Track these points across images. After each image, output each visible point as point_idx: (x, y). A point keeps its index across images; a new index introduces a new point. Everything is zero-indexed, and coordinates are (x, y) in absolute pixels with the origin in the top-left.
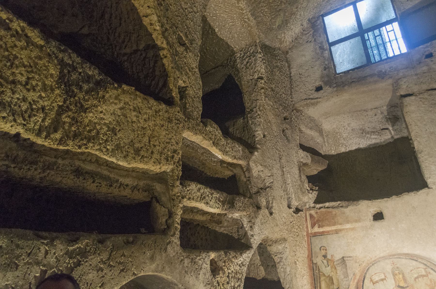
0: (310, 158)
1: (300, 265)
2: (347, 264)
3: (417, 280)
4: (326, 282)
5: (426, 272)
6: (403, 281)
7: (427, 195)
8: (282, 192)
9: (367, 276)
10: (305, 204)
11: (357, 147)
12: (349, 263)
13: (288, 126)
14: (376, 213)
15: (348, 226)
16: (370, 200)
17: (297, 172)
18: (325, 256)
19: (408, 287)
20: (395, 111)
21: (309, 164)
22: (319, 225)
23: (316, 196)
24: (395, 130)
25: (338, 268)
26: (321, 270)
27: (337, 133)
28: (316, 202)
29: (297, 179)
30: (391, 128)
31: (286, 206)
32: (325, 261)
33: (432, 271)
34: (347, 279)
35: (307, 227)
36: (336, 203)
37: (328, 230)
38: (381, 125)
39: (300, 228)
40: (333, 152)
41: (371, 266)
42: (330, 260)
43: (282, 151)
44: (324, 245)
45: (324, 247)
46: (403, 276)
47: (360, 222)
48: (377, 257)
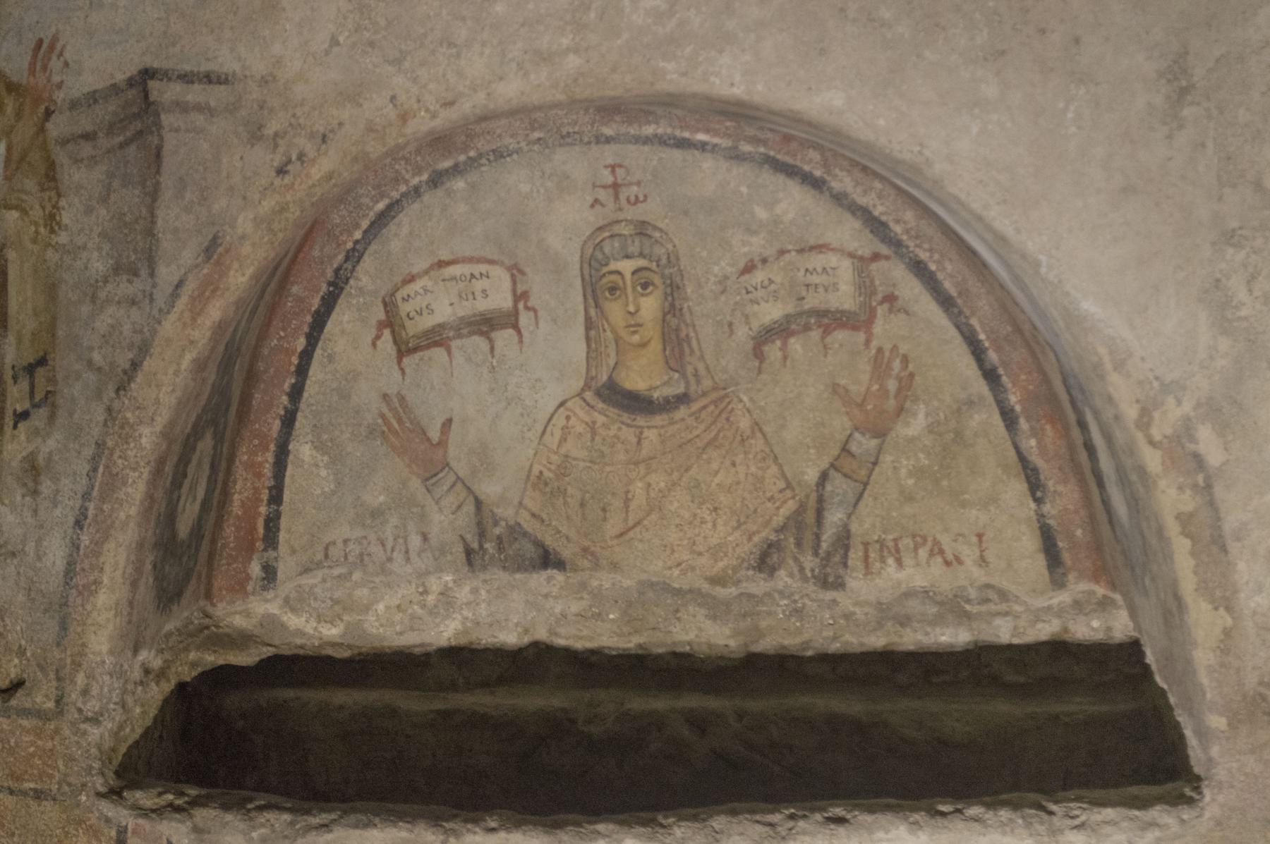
2: (170, 141)
3: (773, 351)
5: (865, 286)
6: (656, 345)
9: (367, 277)
12: (182, 142)
19: (683, 399)
25: (73, 175)
33: (911, 289)
34: (139, 285)
41: (417, 192)
46: (672, 309)
48: (466, 107)
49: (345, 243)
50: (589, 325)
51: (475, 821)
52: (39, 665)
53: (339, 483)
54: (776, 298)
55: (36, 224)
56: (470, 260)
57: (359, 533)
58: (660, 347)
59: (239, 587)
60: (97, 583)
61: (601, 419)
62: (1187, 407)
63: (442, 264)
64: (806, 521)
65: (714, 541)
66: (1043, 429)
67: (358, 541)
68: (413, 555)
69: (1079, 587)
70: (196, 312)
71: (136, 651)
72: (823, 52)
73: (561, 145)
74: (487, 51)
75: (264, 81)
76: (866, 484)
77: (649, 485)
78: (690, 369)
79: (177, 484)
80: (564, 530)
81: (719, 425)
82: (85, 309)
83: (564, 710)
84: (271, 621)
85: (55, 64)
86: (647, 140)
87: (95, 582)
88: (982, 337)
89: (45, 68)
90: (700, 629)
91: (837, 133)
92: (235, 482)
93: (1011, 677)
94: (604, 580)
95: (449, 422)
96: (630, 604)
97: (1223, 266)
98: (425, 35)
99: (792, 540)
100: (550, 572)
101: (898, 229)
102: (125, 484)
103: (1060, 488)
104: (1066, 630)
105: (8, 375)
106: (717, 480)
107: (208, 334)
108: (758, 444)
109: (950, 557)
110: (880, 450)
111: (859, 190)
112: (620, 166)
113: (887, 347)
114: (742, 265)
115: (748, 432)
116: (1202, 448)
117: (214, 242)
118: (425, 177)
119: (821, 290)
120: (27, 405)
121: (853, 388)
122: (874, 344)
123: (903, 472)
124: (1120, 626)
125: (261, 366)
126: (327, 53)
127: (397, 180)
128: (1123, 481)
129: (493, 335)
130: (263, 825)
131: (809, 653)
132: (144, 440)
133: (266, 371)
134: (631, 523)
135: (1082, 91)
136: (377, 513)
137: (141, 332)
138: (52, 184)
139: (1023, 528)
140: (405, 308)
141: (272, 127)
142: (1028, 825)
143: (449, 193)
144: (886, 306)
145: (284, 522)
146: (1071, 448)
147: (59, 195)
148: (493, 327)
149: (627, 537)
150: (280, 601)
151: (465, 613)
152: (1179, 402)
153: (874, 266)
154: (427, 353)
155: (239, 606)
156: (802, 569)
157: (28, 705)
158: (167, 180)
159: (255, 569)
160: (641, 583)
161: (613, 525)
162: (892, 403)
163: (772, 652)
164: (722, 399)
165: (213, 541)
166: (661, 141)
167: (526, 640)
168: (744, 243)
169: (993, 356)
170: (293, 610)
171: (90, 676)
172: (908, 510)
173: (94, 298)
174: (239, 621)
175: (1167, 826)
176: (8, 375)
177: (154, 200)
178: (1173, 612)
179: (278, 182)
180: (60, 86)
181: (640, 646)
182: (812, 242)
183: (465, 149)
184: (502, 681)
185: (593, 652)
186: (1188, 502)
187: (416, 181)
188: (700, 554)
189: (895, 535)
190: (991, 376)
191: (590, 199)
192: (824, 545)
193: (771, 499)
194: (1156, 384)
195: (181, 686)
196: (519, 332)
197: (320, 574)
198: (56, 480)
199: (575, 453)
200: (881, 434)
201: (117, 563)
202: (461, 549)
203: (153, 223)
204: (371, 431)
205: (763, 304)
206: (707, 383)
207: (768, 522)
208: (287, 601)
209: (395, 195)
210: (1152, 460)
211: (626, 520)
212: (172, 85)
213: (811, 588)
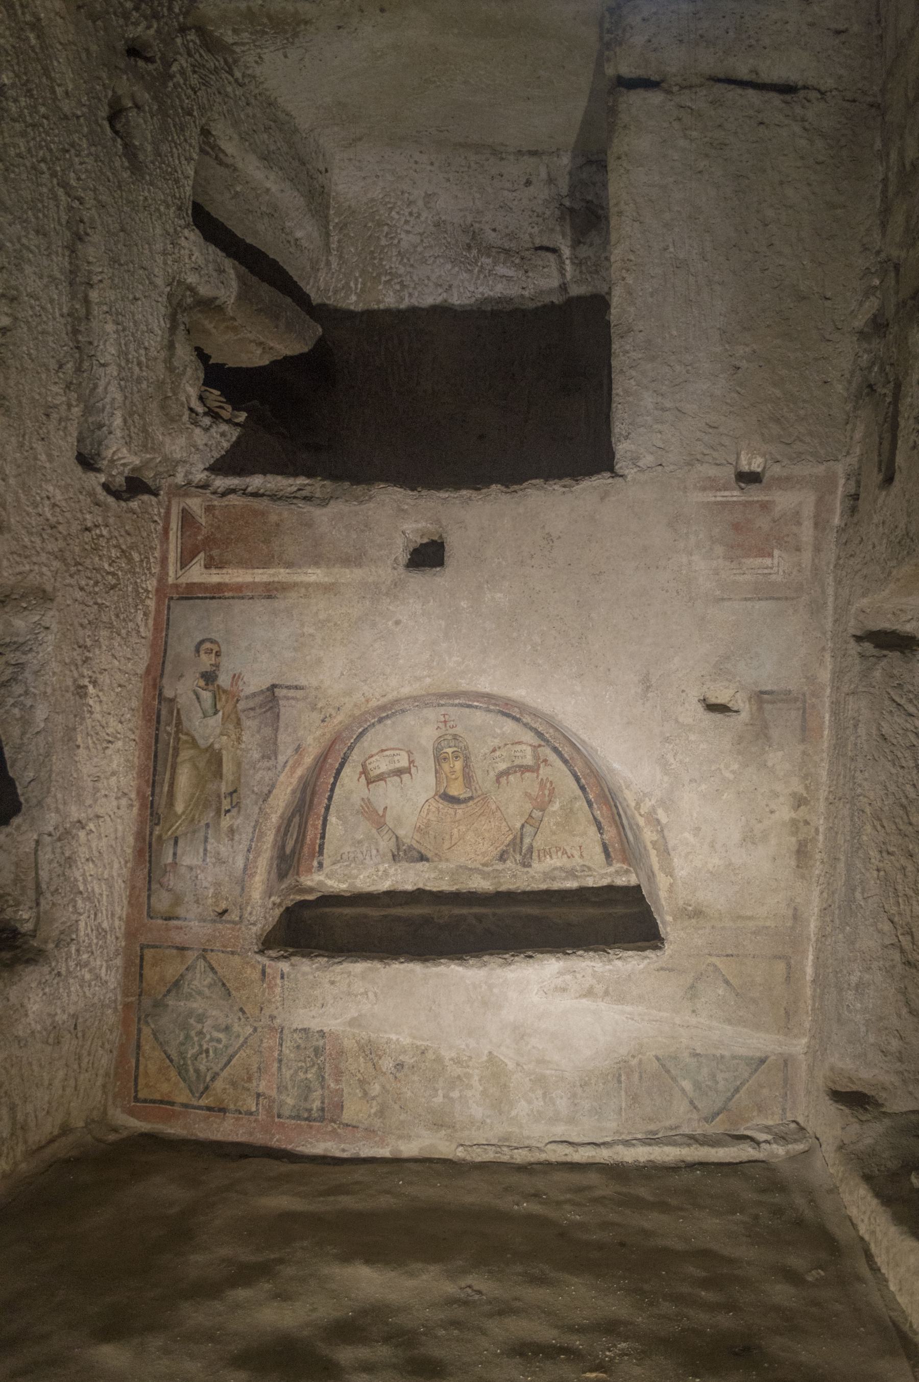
0: (234, 284)
1: (99, 703)
2: (283, 710)
3: (503, 780)
4: (195, 767)
5: (536, 757)
6: (461, 779)
7: (602, 499)
8: (55, 389)
9: (355, 756)
10: (173, 465)
11: (439, 300)
12: (287, 710)
13: (145, 97)
14: (425, 540)
15: (314, 575)
16: (413, 489)
17: (159, 325)
18: (209, 677)
19: (471, 798)
20: (594, 184)
21: (230, 312)
22: (211, 558)
23: (226, 445)
24: (578, 263)
25: (247, 723)
26: (186, 724)
27: (380, 224)
28: (218, 468)
29: (153, 353)
30: (566, 252)
31: (71, 455)
32: (206, 695)
33: (553, 757)
34: (271, 763)
35: (164, 560)
36: (291, 481)
37: (240, 580)
38: (536, 229)
39: (130, 560)
40: (354, 298)
42: (225, 691)
43: (90, 202)
44: (213, 636)
45: (212, 641)
47: (360, 566)
48: (390, 697)
51: (396, 959)
53: (346, 831)
56: (393, 749)
57: (353, 849)
59: (309, 870)
61: (441, 806)
62: (653, 802)
63: (383, 751)
64: (517, 842)
67: (353, 852)
69: (617, 865)
70: (293, 772)
71: (270, 897)
72: (517, 675)
75: (316, 689)
79: (286, 834)
82: (251, 772)
84: (321, 883)
85: (240, 683)
86: (456, 705)
91: (524, 704)
94: (443, 865)
96: (453, 874)
100: (424, 862)
101: (547, 736)
105: (223, 796)
108: (498, 814)
110: (543, 816)
113: (545, 778)
116: (659, 817)
120: (229, 807)
123: (552, 824)
124: (633, 880)
125: (317, 788)
127: (366, 721)
128: (631, 828)
136: (360, 842)
140: (369, 767)
141: (320, 705)
143: (385, 725)
146: (613, 814)
155: (309, 877)
158: (282, 724)
159: (315, 864)
161: (447, 845)
162: (547, 799)
165: (300, 854)
166: (462, 705)
167: (415, 888)
169: (583, 781)
170: (329, 878)
171: (253, 908)
172: (554, 837)
173: (254, 768)
174: (309, 883)
176: (223, 796)
178: (651, 877)
180: (242, 690)
183: (391, 709)
184: (407, 903)
185: (440, 892)
186: (655, 837)
190: (582, 788)
195: (287, 909)
197: (339, 865)
198: (240, 834)
200: (543, 810)
206: (480, 792)
208: (327, 875)
210: (641, 821)
213: (519, 867)
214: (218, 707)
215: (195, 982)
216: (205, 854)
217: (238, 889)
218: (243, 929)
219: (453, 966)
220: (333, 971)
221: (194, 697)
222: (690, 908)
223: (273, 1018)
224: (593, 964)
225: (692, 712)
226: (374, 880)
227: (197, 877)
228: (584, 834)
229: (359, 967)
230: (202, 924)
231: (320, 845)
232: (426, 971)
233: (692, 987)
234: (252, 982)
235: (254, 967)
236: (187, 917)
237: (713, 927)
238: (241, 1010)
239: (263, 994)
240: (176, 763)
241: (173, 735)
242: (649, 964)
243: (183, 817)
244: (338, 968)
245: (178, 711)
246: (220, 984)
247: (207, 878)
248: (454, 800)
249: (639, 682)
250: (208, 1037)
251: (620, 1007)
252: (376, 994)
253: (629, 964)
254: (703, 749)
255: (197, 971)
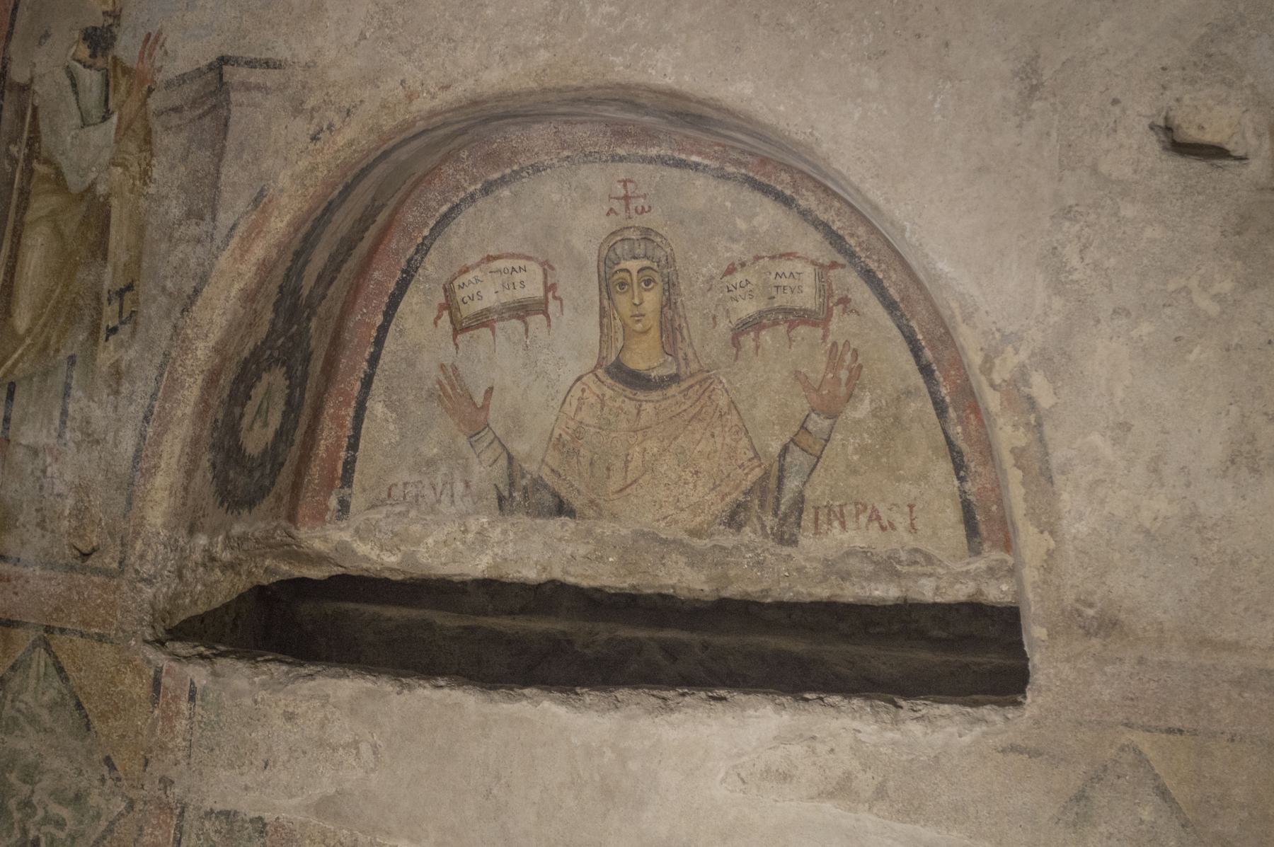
2: (235, 113)
3: (748, 341)
4: (58, 233)
5: (824, 291)
6: (655, 333)
9: (431, 267)
12: (245, 114)
18: (99, 40)
19: (675, 378)
26: (47, 140)
32: (91, 79)
33: (862, 293)
34: (204, 227)
42: (127, 71)
49: (416, 238)
50: (603, 313)
51: (427, 679)
52: (109, 533)
53: (403, 436)
54: (752, 297)
55: (134, 178)
57: (416, 477)
58: (658, 334)
59: (319, 516)
60: (156, 467)
61: (609, 393)
63: (490, 259)
65: (694, 499)
66: (967, 418)
67: (415, 484)
68: (457, 498)
70: (244, 251)
72: (738, 49)
73: (585, 162)
74: (478, 46)
75: (307, 67)
76: (819, 458)
77: (645, 450)
78: (681, 354)
80: (576, 484)
81: (703, 402)
82: (164, 246)
83: (564, 633)
84: (343, 548)
85: (158, 53)
86: (651, 160)
87: (155, 467)
88: (920, 337)
89: (150, 55)
90: (681, 575)
92: (322, 431)
93: (936, 633)
94: (605, 528)
95: (490, 391)
96: (626, 550)
97: (1060, 236)
98: (431, 32)
99: (756, 502)
101: (852, 242)
102: (183, 387)
103: (980, 469)
104: (980, 592)
105: (105, 297)
106: (698, 448)
107: (254, 268)
109: (885, 523)
111: (821, 207)
112: (631, 181)
113: (841, 342)
114: (725, 267)
115: (725, 409)
116: (1035, 391)
117: (261, 194)
118: (479, 186)
119: (788, 291)
120: (116, 322)
121: (811, 375)
122: (830, 339)
123: (850, 448)
125: (347, 336)
126: (356, 45)
127: (457, 188)
129: (528, 319)
130: (264, 673)
131: (769, 600)
132: (199, 353)
133: (351, 341)
134: (629, 482)
135: (949, 85)
136: (431, 463)
137: (203, 265)
138: (148, 147)
139: (948, 501)
140: (461, 294)
141: (311, 102)
142: (876, 714)
143: (497, 200)
144: (841, 306)
145: (358, 465)
147: (152, 155)
148: (528, 313)
149: (625, 493)
150: (352, 530)
151: (496, 550)
152: (1017, 353)
153: (832, 273)
154: (476, 332)
156: (763, 527)
157: (99, 565)
158: (231, 143)
159: (333, 503)
160: (635, 532)
161: (615, 483)
162: (843, 390)
163: (738, 597)
164: (705, 380)
167: (544, 577)
168: (728, 249)
169: (928, 354)
170: (362, 539)
172: (853, 481)
173: (170, 238)
174: (318, 545)
175: (994, 723)
176: (105, 297)
177: (220, 160)
179: (311, 146)
181: (634, 587)
182: (782, 250)
183: (510, 163)
184: (524, 611)
186: (1021, 438)
187: (472, 189)
188: (682, 510)
189: (842, 502)
190: (926, 370)
191: (606, 209)
192: (783, 508)
193: (741, 466)
194: (998, 335)
196: (548, 317)
197: (384, 510)
198: (132, 382)
199: (588, 420)
200: (833, 416)
201: (173, 452)
202: (495, 496)
203: (218, 178)
204: (431, 394)
205: (741, 301)
206: (694, 366)
207: (738, 486)
208: (357, 531)
209: (456, 200)
211: (625, 478)
212: (240, 69)
213: (770, 543)
214: (111, 104)
215: (27, 697)
216: (63, 423)
217: (122, 500)
218: (125, 588)
219: (546, 704)
220: (294, 693)
221: (67, 82)
222: (1091, 612)
223: (166, 782)
224: (856, 724)
225: (1131, 151)
226: (455, 550)
227: (44, 471)
228: (923, 476)
229: (346, 687)
230: (48, 573)
231: (346, 463)
232: (489, 708)
233: (1081, 797)
234: (133, 703)
235: (139, 672)
236: (23, 557)
237: (1141, 661)
238: (108, 761)
239: (152, 732)
240: (23, 224)
241: (21, 164)
242: (985, 734)
243: (28, 341)
244: (305, 687)
245: (35, 109)
246: (72, 703)
247: (62, 475)
248: (635, 380)
249: (1016, 74)
250: (40, 813)
251: (909, 827)
252: (375, 749)
253: (941, 734)
254: (1152, 241)
255: (32, 672)
